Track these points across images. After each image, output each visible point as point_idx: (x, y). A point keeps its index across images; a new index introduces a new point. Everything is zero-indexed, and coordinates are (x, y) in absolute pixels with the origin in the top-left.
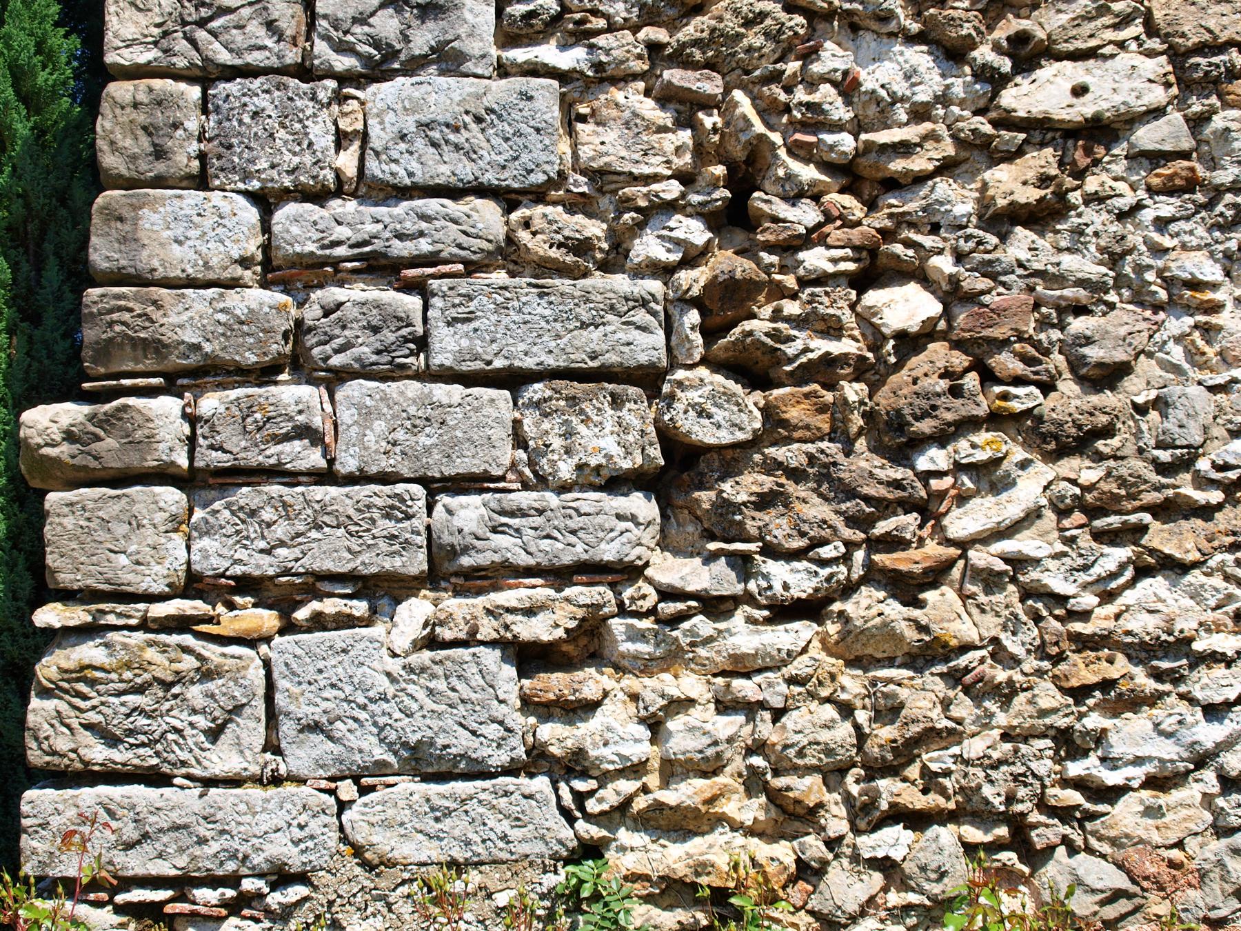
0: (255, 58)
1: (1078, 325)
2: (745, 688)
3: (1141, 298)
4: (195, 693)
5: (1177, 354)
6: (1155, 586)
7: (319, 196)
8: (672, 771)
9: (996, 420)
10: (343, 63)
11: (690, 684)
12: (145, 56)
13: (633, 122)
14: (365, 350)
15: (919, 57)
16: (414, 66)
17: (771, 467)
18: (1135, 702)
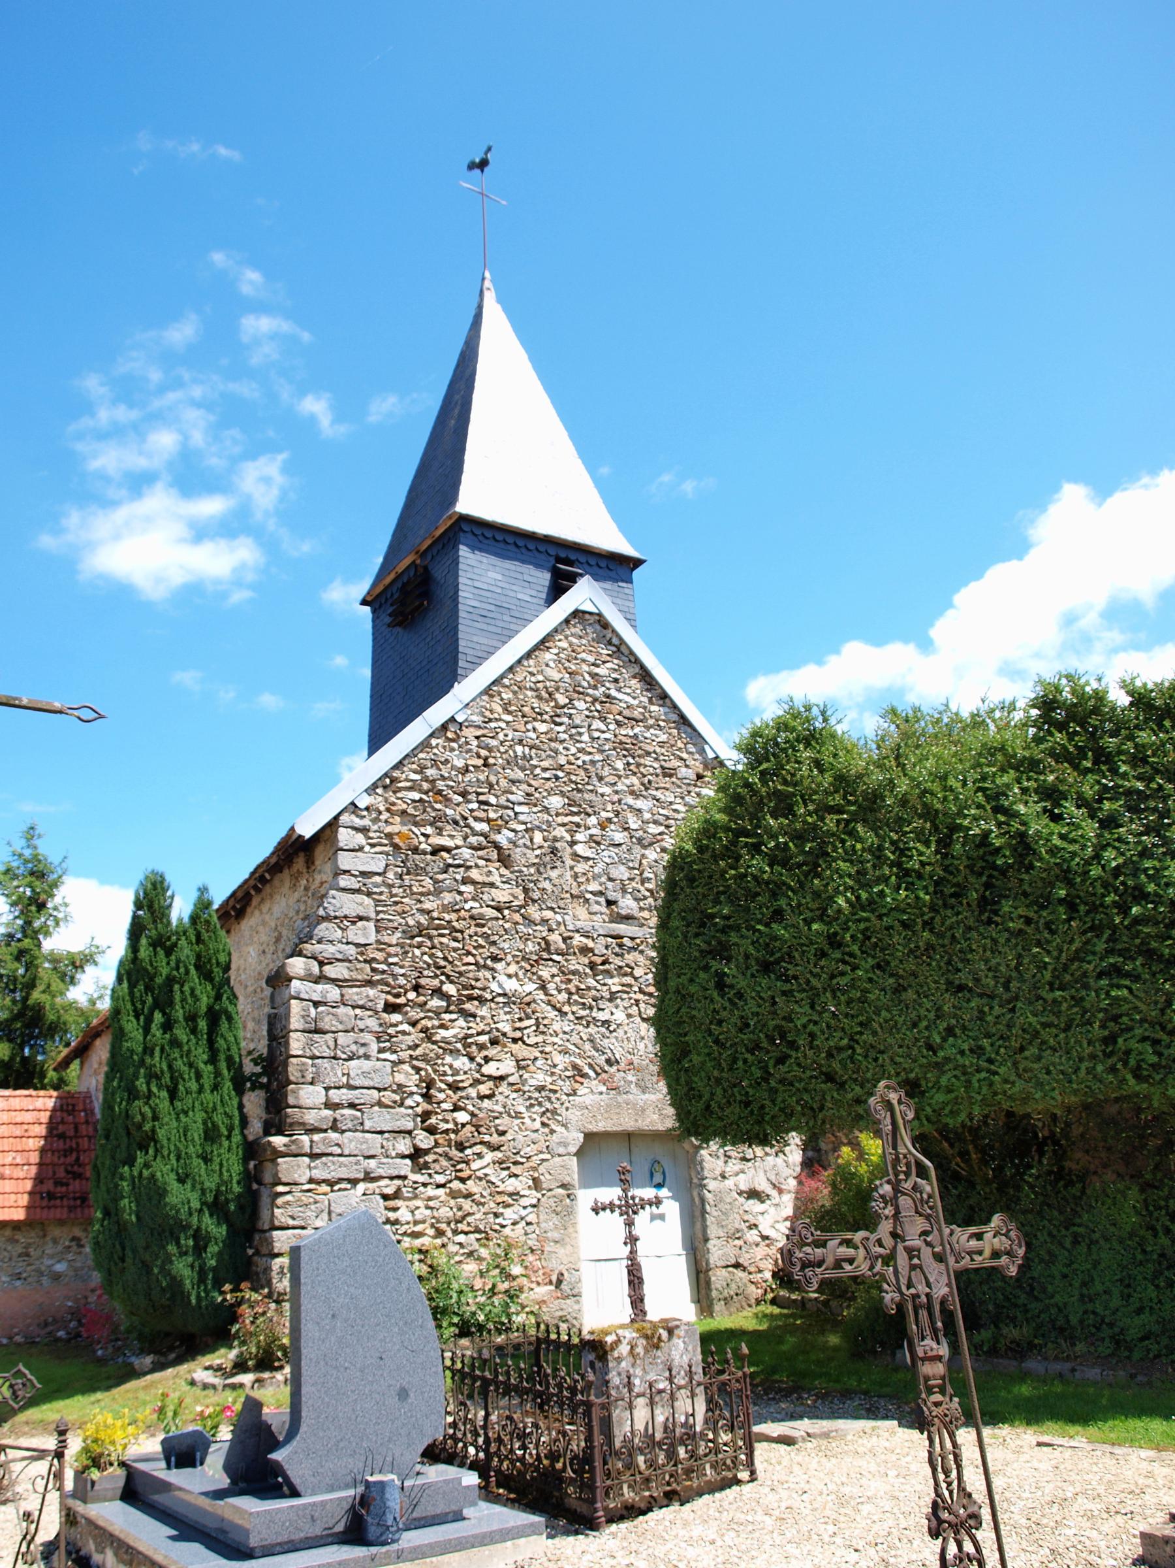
0: (324, 1055)
1: (497, 1121)
2: (431, 1204)
3: (509, 1115)
4: (313, 1207)
5: (516, 1128)
6: (513, 1179)
7: (338, 1088)
9: (481, 1143)
10: (344, 1056)
12: (300, 1053)
13: (407, 1073)
14: (350, 1125)
15: (465, 1059)
16: (359, 1058)
17: (436, 1153)
18: (509, 1206)
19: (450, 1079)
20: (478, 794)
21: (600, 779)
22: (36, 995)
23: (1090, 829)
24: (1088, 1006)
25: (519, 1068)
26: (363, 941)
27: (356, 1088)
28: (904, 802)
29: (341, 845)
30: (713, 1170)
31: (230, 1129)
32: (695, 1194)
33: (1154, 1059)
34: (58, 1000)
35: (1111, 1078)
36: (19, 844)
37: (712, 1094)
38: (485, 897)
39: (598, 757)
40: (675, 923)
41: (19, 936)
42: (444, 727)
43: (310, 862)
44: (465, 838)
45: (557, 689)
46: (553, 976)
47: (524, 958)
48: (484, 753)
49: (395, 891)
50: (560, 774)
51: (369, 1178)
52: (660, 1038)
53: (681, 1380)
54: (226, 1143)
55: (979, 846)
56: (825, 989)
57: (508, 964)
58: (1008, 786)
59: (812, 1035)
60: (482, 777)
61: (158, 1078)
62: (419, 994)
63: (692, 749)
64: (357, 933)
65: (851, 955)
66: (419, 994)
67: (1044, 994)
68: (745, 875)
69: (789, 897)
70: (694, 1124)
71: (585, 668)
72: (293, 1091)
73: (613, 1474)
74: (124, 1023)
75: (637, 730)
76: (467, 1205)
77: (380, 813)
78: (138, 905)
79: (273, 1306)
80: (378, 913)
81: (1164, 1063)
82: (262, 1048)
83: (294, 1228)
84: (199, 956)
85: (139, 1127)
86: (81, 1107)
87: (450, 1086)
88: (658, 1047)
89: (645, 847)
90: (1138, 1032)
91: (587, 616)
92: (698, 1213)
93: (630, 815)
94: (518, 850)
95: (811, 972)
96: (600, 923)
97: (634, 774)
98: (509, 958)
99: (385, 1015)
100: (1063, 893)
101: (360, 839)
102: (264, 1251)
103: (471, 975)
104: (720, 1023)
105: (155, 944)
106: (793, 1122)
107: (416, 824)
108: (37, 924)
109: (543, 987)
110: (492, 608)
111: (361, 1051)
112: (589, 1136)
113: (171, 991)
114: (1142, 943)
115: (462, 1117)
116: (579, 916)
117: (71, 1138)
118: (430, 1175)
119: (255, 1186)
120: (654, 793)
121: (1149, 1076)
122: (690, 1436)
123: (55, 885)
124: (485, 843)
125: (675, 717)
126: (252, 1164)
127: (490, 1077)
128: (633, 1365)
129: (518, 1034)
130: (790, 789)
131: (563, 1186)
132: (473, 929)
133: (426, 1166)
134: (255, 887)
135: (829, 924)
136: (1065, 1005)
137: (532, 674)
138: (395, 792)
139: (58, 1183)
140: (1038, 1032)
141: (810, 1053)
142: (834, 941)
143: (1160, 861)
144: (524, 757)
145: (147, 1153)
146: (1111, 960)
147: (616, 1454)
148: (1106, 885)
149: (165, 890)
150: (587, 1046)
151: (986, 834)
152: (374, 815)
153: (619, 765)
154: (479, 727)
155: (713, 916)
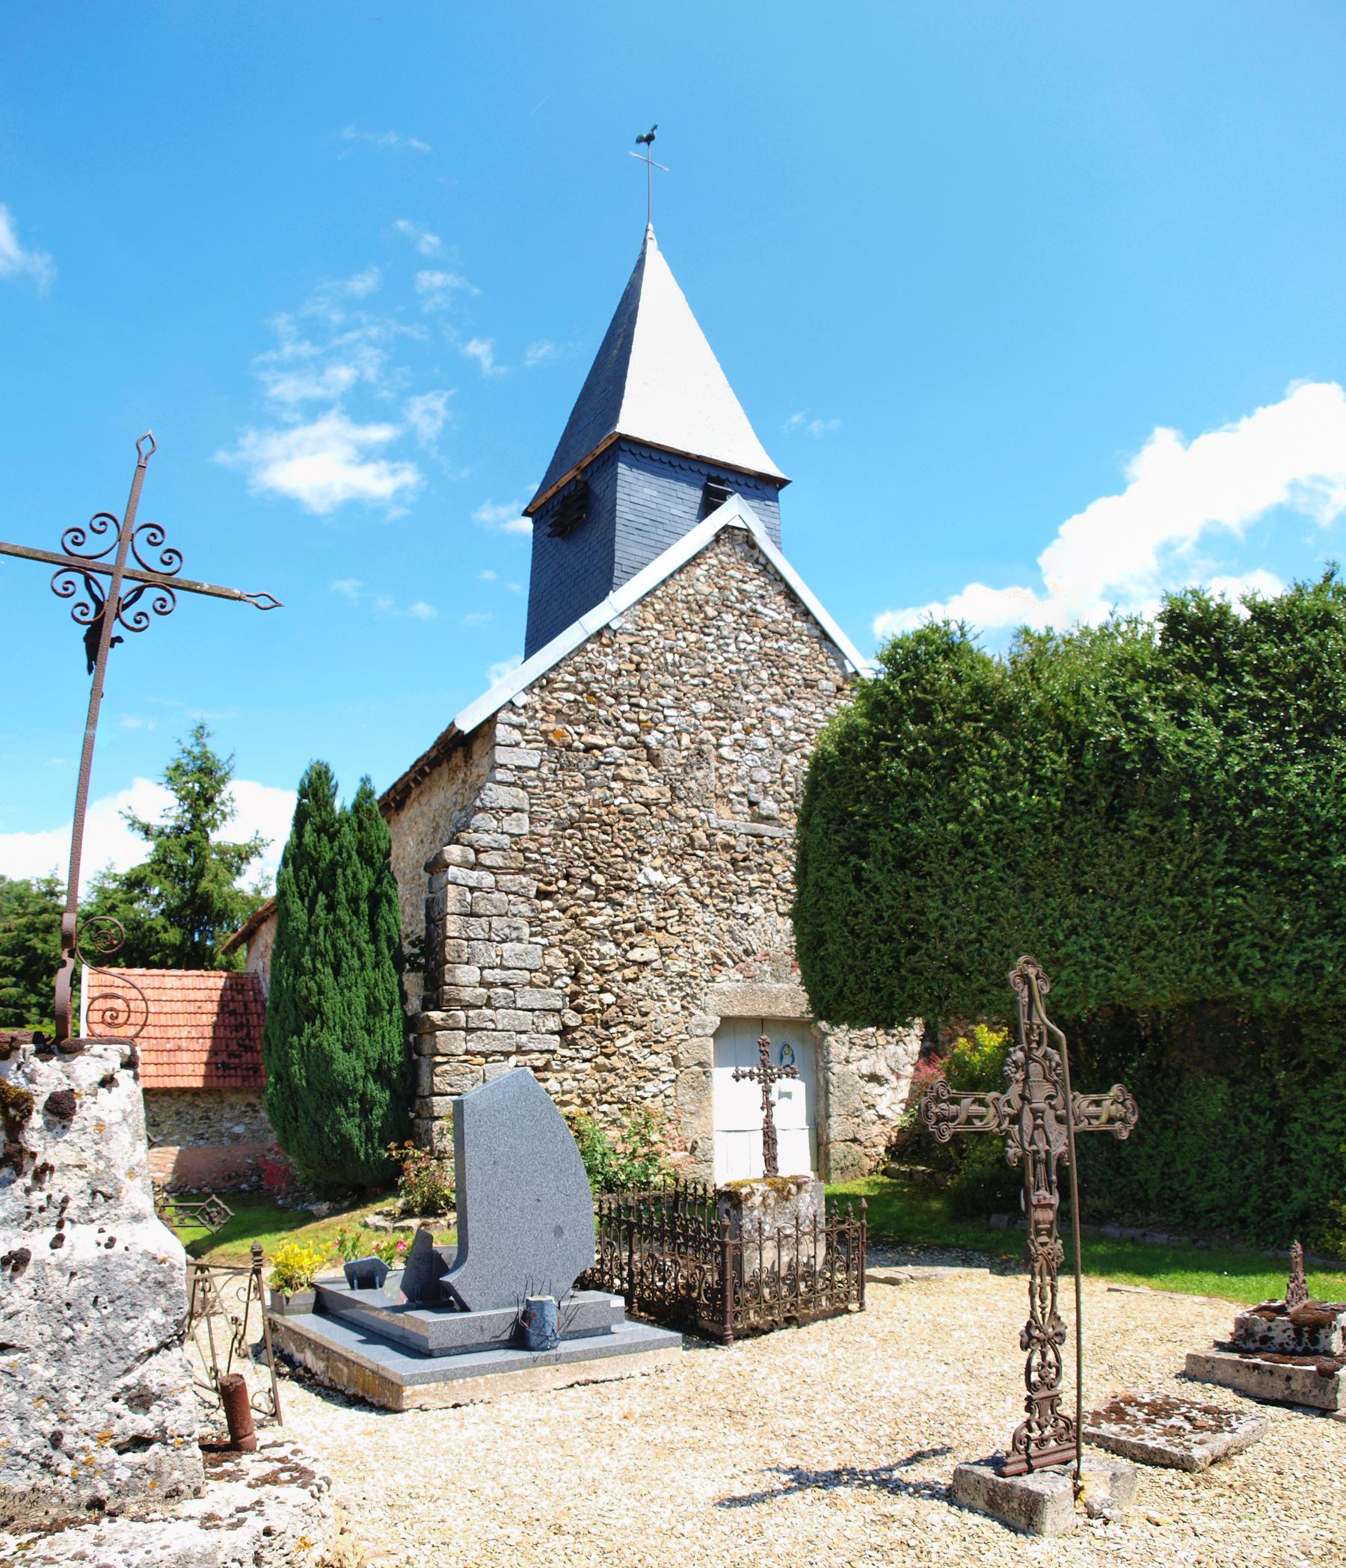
2: (578, 1076)
3: (652, 998)
4: (469, 1076)
7: (492, 968)
8: (564, 1093)
9: (625, 1022)
11: (566, 1075)
12: (456, 934)
13: (557, 956)
14: (503, 1003)
15: (612, 945)
16: (512, 940)
18: (650, 1080)
19: (597, 963)
20: (630, 697)
21: (746, 687)
22: (205, 884)
23: (1215, 735)
24: (1204, 912)
25: (662, 954)
26: (516, 831)
27: (509, 969)
28: (1038, 713)
29: (498, 740)
30: (838, 1055)
31: (391, 1004)
32: (821, 1076)
33: (1261, 964)
34: (225, 889)
35: (1219, 979)
36: (189, 742)
37: (845, 981)
38: (634, 794)
39: (744, 667)
40: (817, 820)
41: (188, 828)
42: (599, 634)
43: (468, 757)
44: (617, 737)
45: (707, 602)
46: (696, 870)
47: (669, 852)
48: (636, 658)
49: (548, 785)
50: (708, 681)
51: (520, 1051)
52: (797, 930)
53: (805, 1228)
54: (387, 1017)
55: (1109, 752)
56: (957, 886)
57: (654, 858)
58: (1138, 695)
59: (943, 929)
60: (634, 681)
61: (322, 955)
62: (569, 883)
63: (832, 663)
64: (510, 824)
65: (984, 854)
66: (569, 883)
67: (1164, 899)
68: (885, 777)
69: (926, 798)
70: (827, 1008)
71: (734, 584)
72: (450, 970)
73: (742, 1302)
74: (289, 904)
75: (781, 643)
76: (611, 1078)
77: (536, 711)
78: (303, 794)
79: (434, 1162)
80: (532, 805)
81: (1269, 968)
82: (420, 930)
83: (452, 1094)
84: (360, 843)
85: (306, 1000)
86: (249, 986)
87: (597, 969)
88: (794, 938)
89: (787, 753)
90: (1249, 938)
91: (736, 532)
92: (822, 1093)
93: (773, 722)
94: (666, 750)
95: (944, 869)
96: (742, 823)
97: (778, 684)
98: (656, 852)
99: (537, 901)
100: (1187, 796)
101: (516, 735)
102: (425, 1114)
103: (619, 866)
104: (856, 914)
105: (319, 830)
106: (919, 1009)
107: (570, 723)
108: (205, 818)
109: (687, 881)
110: (647, 522)
111: (514, 935)
112: (726, 1020)
113: (335, 875)
114: (1259, 856)
115: (608, 998)
116: (721, 816)
117: (241, 1015)
118: (577, 1050)
119: (415, 1057)
120: (796, 702)
121: (1254, 980)
122: (810, 1274)
123: (222, 781)
124: (635, 743)
125: (817, 633)
126: (411, 1037)
127: (635, 962)
128: (764, 1214)
129: (662, 923)
130: (930, 697)
131: (700, 1064)
132: (622, 823)
133: (574, 1042)
134: (415, 780)
135: (963, 824)
136: (1182, 911)
137: (683, 588)
138: (550, 692)
139: (231, 1055)
140: (1155, 934)
141: (940, 945)
142: (968, 841)
143: (1280, 766)
144: (674, 664)
145: (314, 1024)
146: (1229, 870)
147: (746, 1286)
148: (1228, 789)
149: (329, 780)
150: (727, 937)
151: (1116, 740)
152: (530, 713)
153: (764, 675)
154: (632, 634)
155: (852, 815)
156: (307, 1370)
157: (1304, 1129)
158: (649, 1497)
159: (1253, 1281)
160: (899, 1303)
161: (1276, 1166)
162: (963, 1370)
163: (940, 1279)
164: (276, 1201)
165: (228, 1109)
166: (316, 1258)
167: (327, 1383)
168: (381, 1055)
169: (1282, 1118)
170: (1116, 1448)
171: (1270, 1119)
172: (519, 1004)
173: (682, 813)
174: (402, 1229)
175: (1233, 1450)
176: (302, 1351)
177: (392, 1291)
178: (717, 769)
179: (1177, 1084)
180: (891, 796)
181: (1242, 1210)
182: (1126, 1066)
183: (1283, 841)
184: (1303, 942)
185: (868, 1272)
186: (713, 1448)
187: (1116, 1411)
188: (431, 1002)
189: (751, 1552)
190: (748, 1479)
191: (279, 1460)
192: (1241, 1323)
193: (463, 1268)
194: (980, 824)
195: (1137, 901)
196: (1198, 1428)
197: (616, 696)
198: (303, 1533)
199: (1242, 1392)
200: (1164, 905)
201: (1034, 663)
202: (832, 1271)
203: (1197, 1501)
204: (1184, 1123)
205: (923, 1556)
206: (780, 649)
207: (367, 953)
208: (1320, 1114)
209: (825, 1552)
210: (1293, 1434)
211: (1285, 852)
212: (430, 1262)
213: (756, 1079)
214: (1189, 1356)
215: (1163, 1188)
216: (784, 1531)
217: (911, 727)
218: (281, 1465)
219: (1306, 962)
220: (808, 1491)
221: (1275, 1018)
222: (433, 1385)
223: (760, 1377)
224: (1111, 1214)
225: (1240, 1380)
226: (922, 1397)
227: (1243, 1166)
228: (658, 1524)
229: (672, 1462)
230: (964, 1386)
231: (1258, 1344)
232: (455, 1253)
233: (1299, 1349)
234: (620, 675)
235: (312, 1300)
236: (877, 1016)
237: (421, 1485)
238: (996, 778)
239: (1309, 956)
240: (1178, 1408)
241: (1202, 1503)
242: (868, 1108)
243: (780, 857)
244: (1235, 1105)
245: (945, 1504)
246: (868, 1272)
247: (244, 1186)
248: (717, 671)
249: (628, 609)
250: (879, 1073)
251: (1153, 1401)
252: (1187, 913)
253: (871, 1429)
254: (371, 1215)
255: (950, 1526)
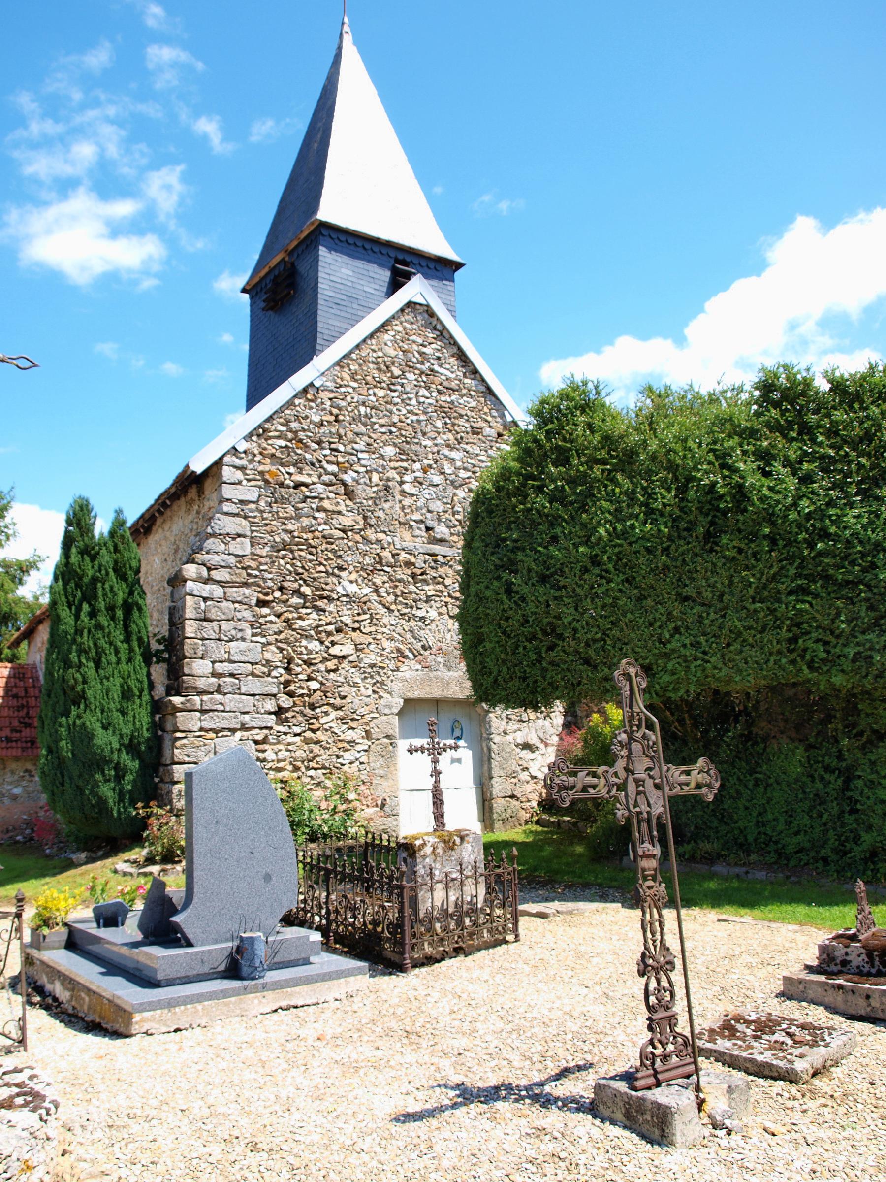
2: (290, 747)
7: (222, 662)
8: (279, 761)
9: (328, 704)
11: (281, 747)
13: (273, 652)
14: (230, 690)
15: (317, 643)
18: (347, 750)
19: (305, 657)
20: (330, 443)
21: (424, 434)
24: (779, 615)
25: (357, 650)
26: (241, 553)
27: (235, 662)
28: (653, 458)
29: (225, 479)
31: (141, 691)
32: (484, 745)
33: (823, 655)
35: (791, 667)
37: (499, 671)
38: (334, 522)
39: (423, 417)
40: (477, 544)
42: (305, 391)
43: (201, 492)
44: (320, 476)
45: (393, 363)
46: (384, 583)
47: (362, 569)
48: (335, 411)
49: (265, 515)
50: (394, 429)
51: (244, 728)
52: (463, 630)
53: (468, 872)
54: (138, 701)
55: (708, 493)
56: (586, 597)
59: (575, 630)
60: (333, 430)
61: (86, 652)
62: (283, 594)
63: (495, 413)
65: (607, 571)
66: (283, 594)
67: (748, 605)
68: (531, 510)
71: (415, 347)
73: (418, 935)
74: (60, 611)
75: (453, 397)
76: (316, 749)
77: (255, 455)
78: (69, 522)
79: (174, 818)
80: (252, 532)
81: (830, 658)
82: (165, 631)
84: (116, 562)
85: (73, 688)
87: (305, 662)
89: (456, 488)
90: (814, 635)
92: (486, 759)
93: (445, 463)
96: (420, 544)
97: (450, 431)
98: (351, 568)
101: (239, 475)
102: (167, 779)
103: (322, 580)
104: (507, 619)
106: (557, 693)
107: (282, 465)
109: (376, 591)
110: (344, 297)
111: (239, 635)
112: (408, 701)
113: (96, 588)
115: (314, 685)
116: (404, 539)
120: (465, 446)
122: (473, 910)
125: (483, 388)
126: (157, 717)
127: (335, 657)
129: (356, 625)
131: (388, 737)
132: (324, 546)
133: (287, 720)
134: (159, 511)
135: (592, 547)
136: (761, 615)
137: (374, 351)
138: (266, 440)
140: (741, 633)
141: (573, 643)
142: (595, 561)
144: (366, 416)
150: (408, 635)
151: (714, 484)
153: (439, 424)
154: (332, 391)
155: (504, 540)
156: (55, 999)
157: (865, 785)
158: (335, 1114)
159: (836, 910)
160: (548, 935)
161: (846, 815)
162: (601, 993)
163: (581, 913)
164: (44, 850)
165: (9, 775)
166: (71, 901)
167: (70, 1011)
168: (133, 732)
169: (848, 776)
170: (732, 1062)
171: (839, 777)
172: (243, 691)
173: (373, 537)
174: (145, 875)
175: (829, 1063)
176: (52, 982)
177: (131, 930)
178: (400, 502)
179: (765, 749)
180: (535, 525)
181: (823, 851)
182: (723, 735)
183: (841, 559)
184: (856, 637)
185: (521, 907)
186: (391, 1067)
187: (728, 1028)
188: (172, 689)
189: (422, 1166)
190: (421, 1095)
191: (17, 1085)
192: (824, 949)
193: (189, 910)
194: (605, 547)
195: (726, 608)
196: (798, 1043)
197: (319, 443)
198: (27, 1157)
199: (832, 1009)
200: (748, 610)
201: (652, 416)
202: (491, 908)
203: (804, 1111)
204: (771, 781)
205: (572, 1168)
206: (452, 402)
207: (122, 651)
208: (877, 772)
209: (487, 1165)
210: (878, 1047)
211: (843, 567)
212: (163, 905)
213: (426, 752)
214: (785, 978)
215: (759, 833)
216: (452, 1145)
217: (553, 469)
218: (16, 1090)
219: (859, 653)
220: (472, 1106)
221: (837, 696)
222: (159, 1012)
223: (433, 1000)
224: (719, 856)
225: (829, 999)
226: (567, 1017)
227: (820, 815)
228: (341, 1140)
229: (356, 1080)
230: (602, 1008)
231: (839, 967)
232: (183, 895)
233: (873, 971)
234: (322, 425)
235: (65, 937)
236: (524, 700)
237: (140, 1105)
238: (618, 510)
239: (861, 649)
240: (779, 1025)
241: (809, 1112)
242: (523, 770)
243: (450, 572)
244: (811, 766)
245: (590, 1117)
246: (521, 907)
247: (19, 838)
248: (401, 421)
249: (328, 370)
250: (531, 742)
251: (759, 1019)
252: (766, 616)
253: (525, 1047)
254: (120, 862)
255: (594, 1137)
